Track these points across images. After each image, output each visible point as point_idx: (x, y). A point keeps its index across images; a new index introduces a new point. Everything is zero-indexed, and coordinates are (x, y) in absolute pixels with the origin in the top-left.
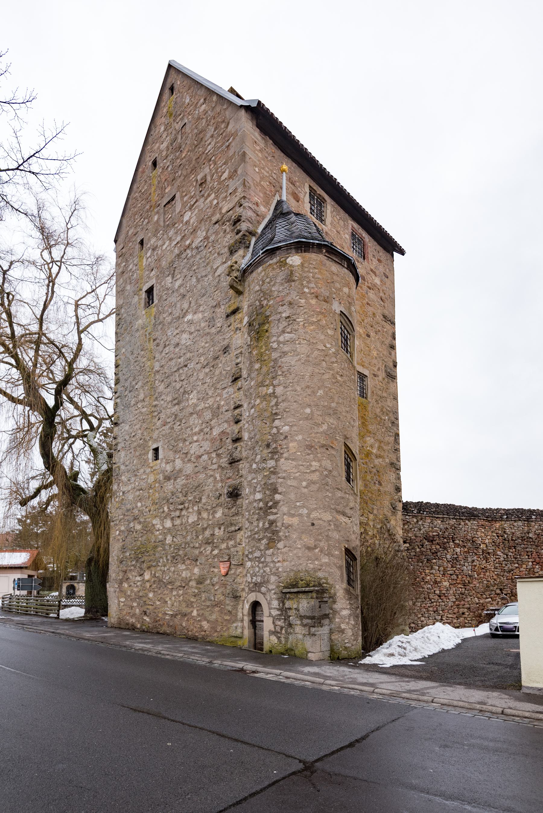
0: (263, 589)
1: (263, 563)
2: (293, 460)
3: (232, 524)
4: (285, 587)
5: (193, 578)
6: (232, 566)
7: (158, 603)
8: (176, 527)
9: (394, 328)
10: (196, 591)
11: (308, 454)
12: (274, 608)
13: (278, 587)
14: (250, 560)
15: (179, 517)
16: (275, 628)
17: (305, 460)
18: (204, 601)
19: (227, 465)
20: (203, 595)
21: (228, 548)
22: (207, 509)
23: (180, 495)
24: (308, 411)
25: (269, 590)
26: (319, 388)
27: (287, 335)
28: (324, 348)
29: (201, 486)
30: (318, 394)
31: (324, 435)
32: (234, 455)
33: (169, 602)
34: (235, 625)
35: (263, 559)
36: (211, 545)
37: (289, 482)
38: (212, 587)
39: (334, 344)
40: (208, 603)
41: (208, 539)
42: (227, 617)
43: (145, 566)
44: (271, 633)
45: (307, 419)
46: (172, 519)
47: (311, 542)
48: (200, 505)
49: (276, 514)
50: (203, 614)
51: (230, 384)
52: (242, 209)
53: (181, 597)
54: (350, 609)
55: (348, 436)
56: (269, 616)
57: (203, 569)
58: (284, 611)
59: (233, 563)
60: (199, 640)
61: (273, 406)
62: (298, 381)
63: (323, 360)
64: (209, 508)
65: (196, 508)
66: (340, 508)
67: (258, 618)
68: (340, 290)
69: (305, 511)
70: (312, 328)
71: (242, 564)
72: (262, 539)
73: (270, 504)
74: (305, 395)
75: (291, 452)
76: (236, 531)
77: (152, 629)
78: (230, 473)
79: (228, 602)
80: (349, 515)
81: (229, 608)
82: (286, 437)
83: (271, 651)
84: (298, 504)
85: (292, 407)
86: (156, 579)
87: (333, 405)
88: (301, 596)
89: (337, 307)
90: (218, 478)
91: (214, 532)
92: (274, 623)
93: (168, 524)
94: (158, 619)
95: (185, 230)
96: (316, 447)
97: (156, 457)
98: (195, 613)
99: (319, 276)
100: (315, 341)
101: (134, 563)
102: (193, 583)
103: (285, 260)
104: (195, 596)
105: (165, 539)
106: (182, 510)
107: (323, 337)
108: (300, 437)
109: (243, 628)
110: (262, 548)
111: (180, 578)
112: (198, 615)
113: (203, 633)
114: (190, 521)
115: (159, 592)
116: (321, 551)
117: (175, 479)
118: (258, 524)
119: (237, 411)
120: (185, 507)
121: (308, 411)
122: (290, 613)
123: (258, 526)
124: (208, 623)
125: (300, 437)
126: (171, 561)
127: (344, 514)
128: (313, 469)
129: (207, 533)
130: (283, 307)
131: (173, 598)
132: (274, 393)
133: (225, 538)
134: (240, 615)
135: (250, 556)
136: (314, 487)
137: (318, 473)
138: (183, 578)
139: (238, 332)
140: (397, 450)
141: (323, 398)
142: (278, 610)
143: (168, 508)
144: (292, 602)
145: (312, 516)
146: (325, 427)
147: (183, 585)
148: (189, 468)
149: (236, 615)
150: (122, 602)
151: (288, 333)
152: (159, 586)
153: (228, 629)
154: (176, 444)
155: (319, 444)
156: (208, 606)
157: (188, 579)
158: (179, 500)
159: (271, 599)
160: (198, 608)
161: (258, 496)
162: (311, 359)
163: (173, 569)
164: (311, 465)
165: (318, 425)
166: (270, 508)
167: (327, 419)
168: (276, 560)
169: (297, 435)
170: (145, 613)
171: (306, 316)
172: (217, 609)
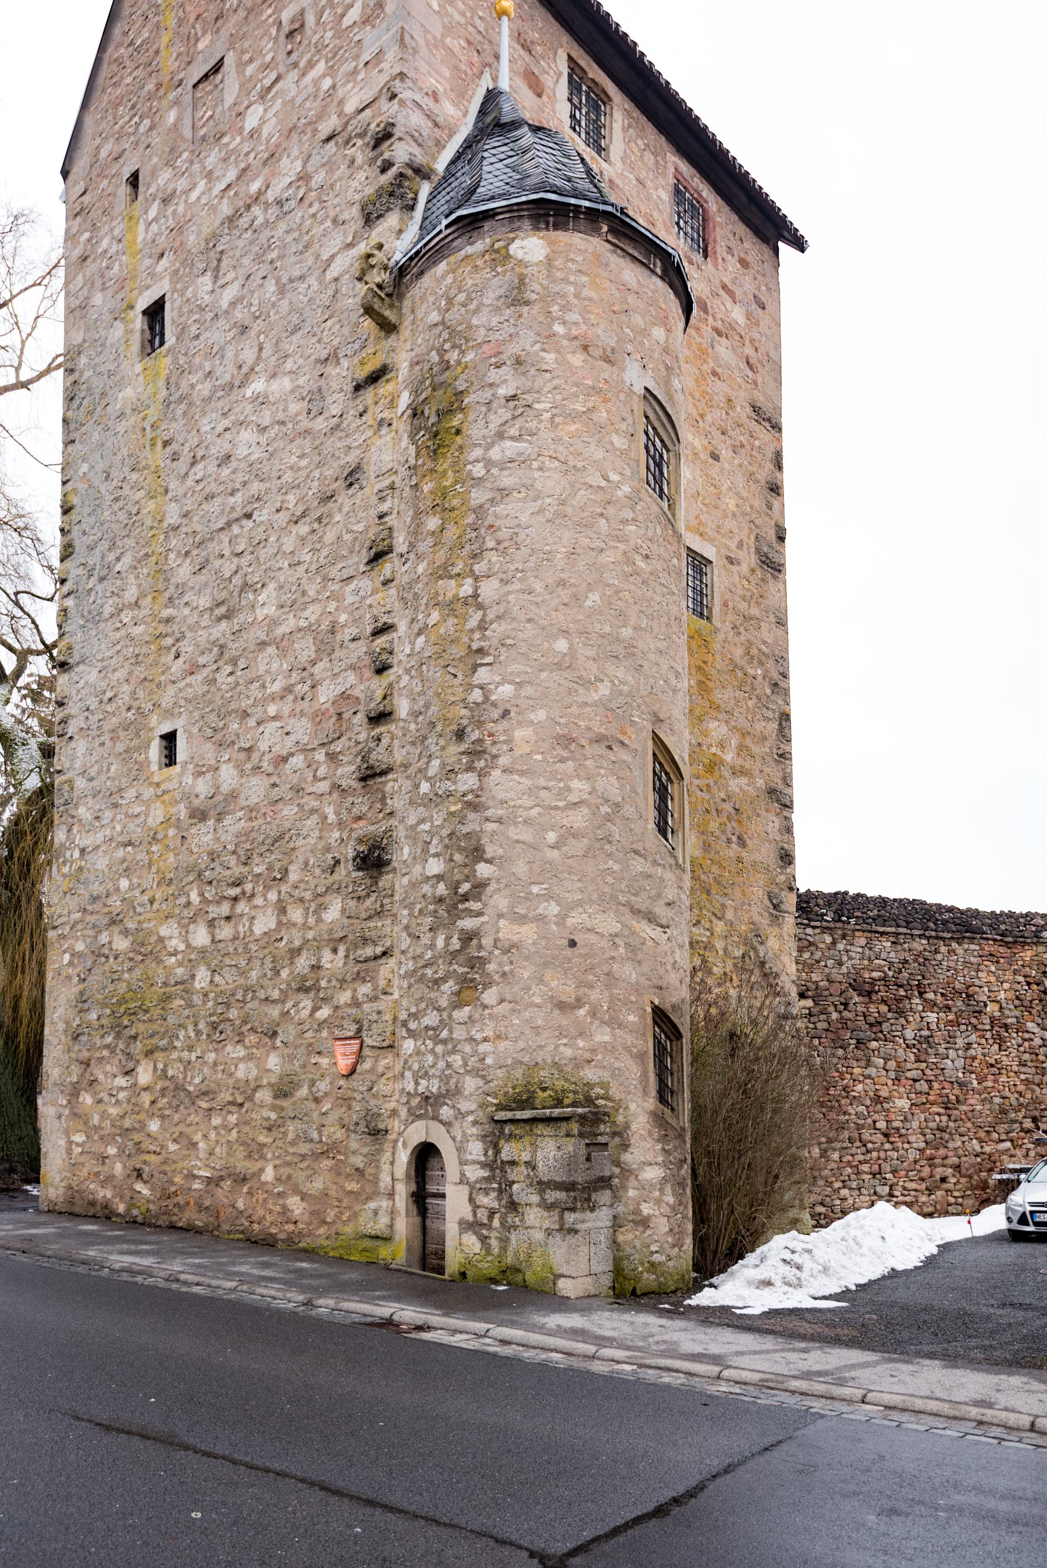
0: (445, 1112)
1: (444, 1042)
2: (523, 773)
3: (365, 940)
4: (501, 1107)
5: (265, 1082)
6: (366, 1052)
7: (173, 1147)
8: (221, 945)
9: (779, 440)
10: (273, 1116)
11: (562, 761)
12: (474, 1162)
13: (483, 1106)
14: (412, 1034)
15: (228, 918)
16: (475, 1214)
17: (553, 775)
18: (293, 1143)
19: (355, 784)
20: (291, 1128)
21: (356, 1003)
22: (302, 900)
23: (233, 861)
24: (562, 645)
25: (461, 1115)
26: (590, 588)
27: (509, 443)
28: (603, 483)
29: (287, 837)
30: (588, 603)
31: (602, 710)
32: (373, 756)
33: (201, 1145)
34: (372, 1205)
35: (444, 1034)
36: (312, 994)
37: (513, 833)
38: (313, 1105)
39: (628, 472)
40: (304, 1148)
41: (304, 978)
42: (353, 1186)
43: (138, 1047)
44: (466, 1226)
45: (559, 666)
46: (211, 924)
47: (568, 991)
48: (283, 889)
49: (480, 914)
50: (289, 1177)
51: (362, 568)
52: (396, 107)
53: (234, 1133)
54: (664, 1164)
55: (662, 716)
56: (461, 1182)
57: (291, 1058)
58: (498, 1169)
59: (368, 1041)
60: (280, 1245)
61: (472, 631)
62: (537, 568)
63: (602, 515)
64: (308, 895)
65: (273, 896)
66: (640, 902)
67: (432, 1188)
68: (645, 332)
69: (553, 909)
70: (573, 428)
71: (391, 1046)
72: (444, 980)
73: (465, 887)
74: (554, 603)
75: (517, 752)
76: (376, 958)
77: (157, 1217)
78: (361, 804)
79: (354, 1145)
80: (664, 922)
81: (358, 1161)
82: (506, 713)
83: (463, 1275)
84: (535, 889)
85: (521, 635)
86: (167, 1084)
87: (626, 633)
88: (540, 1129)
89: (636, 378)
90: (332, 818)
91: (319, 960)
92: (471, 1200)
93: (201, 937)
94: (173, 1189)
95: (247, 154)
96: (583, 742)
97: (170, 759)
98: (269, 1175)
99: (592, 294)
100: (579, 465)
101: (109, 1039)
102: (264, 1096)
103: (506, 247)
104: (269, 1129)
105: (193, 977)
106: (235, 899)
107: (599, 454)
108: (541, 715)
109: (393, 1213)
110: (444, 1003)
111: (231, 1082)
112: (278, 1179)
113: (290, 1227)
114: (259, 929)
115: (176, 1117)
116: (593, 1013)
117: (220, 817)
118: (434, 939)
119: (381, 641)
120: (244, 893)
121: (562, 645)
122: (513, 1174)
123: (432, 946)
124: (302, 1199)
125: (541, 715)
126: (208, 1036)
127: (651, 918)
128: (573, 798)
129: (303, 963)
130: (501, 371)
131: (213, 1135)
132: (475, 596)
133: (349, 978)
134: (385, 1180)
135: (413, 1025)
136: (576, 847)
137: (585, 810)
138: (237, 1080)
139: (384, 430)
140: (784, 757)
141: (600, 613)
142: (484, 1165)
143: (201, 894)
144: (520, 1145)
145: (570, 922)
146: (604, 689)
147: (240, 1100)
148: (255, 790)
149: (376, 1180)
150: (77, 1145)
151: (512, 438)
152: (175, 1102)
153: (355, 1215)
154: (221, 724)
155: (589, 735)
156: (303, 1157)
157: (252, 1085)
158: (228, 873)
159: (466, 1139)
160: (278, 1162)
161: (435, 867)
162: (569, 510)
163: (211, 1057)
164: (569, 790)
165: (588, 684)
166: (465, 898)
167: (610, 668)
168: (478, 1036)
169: (533, 708)
170: (139, 1174)
171: (559, 397)
172: (326, 1163)
